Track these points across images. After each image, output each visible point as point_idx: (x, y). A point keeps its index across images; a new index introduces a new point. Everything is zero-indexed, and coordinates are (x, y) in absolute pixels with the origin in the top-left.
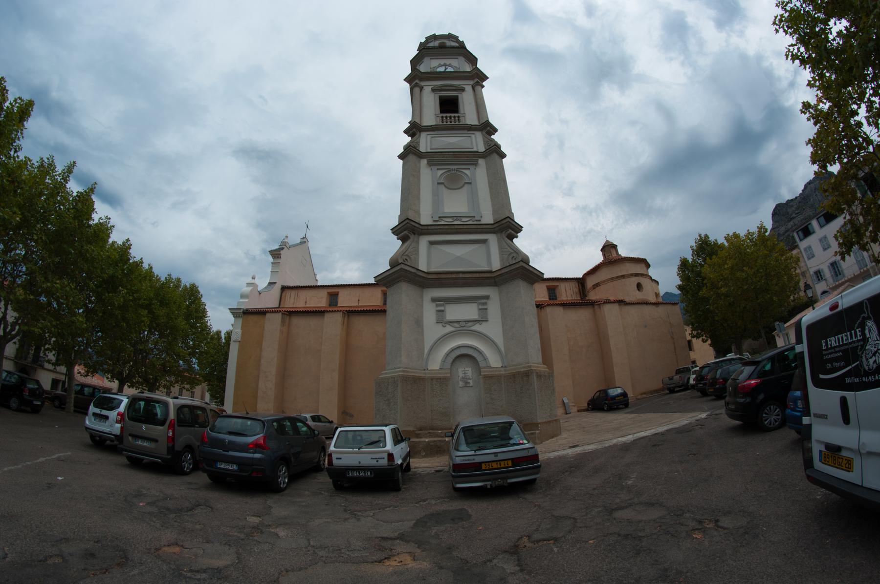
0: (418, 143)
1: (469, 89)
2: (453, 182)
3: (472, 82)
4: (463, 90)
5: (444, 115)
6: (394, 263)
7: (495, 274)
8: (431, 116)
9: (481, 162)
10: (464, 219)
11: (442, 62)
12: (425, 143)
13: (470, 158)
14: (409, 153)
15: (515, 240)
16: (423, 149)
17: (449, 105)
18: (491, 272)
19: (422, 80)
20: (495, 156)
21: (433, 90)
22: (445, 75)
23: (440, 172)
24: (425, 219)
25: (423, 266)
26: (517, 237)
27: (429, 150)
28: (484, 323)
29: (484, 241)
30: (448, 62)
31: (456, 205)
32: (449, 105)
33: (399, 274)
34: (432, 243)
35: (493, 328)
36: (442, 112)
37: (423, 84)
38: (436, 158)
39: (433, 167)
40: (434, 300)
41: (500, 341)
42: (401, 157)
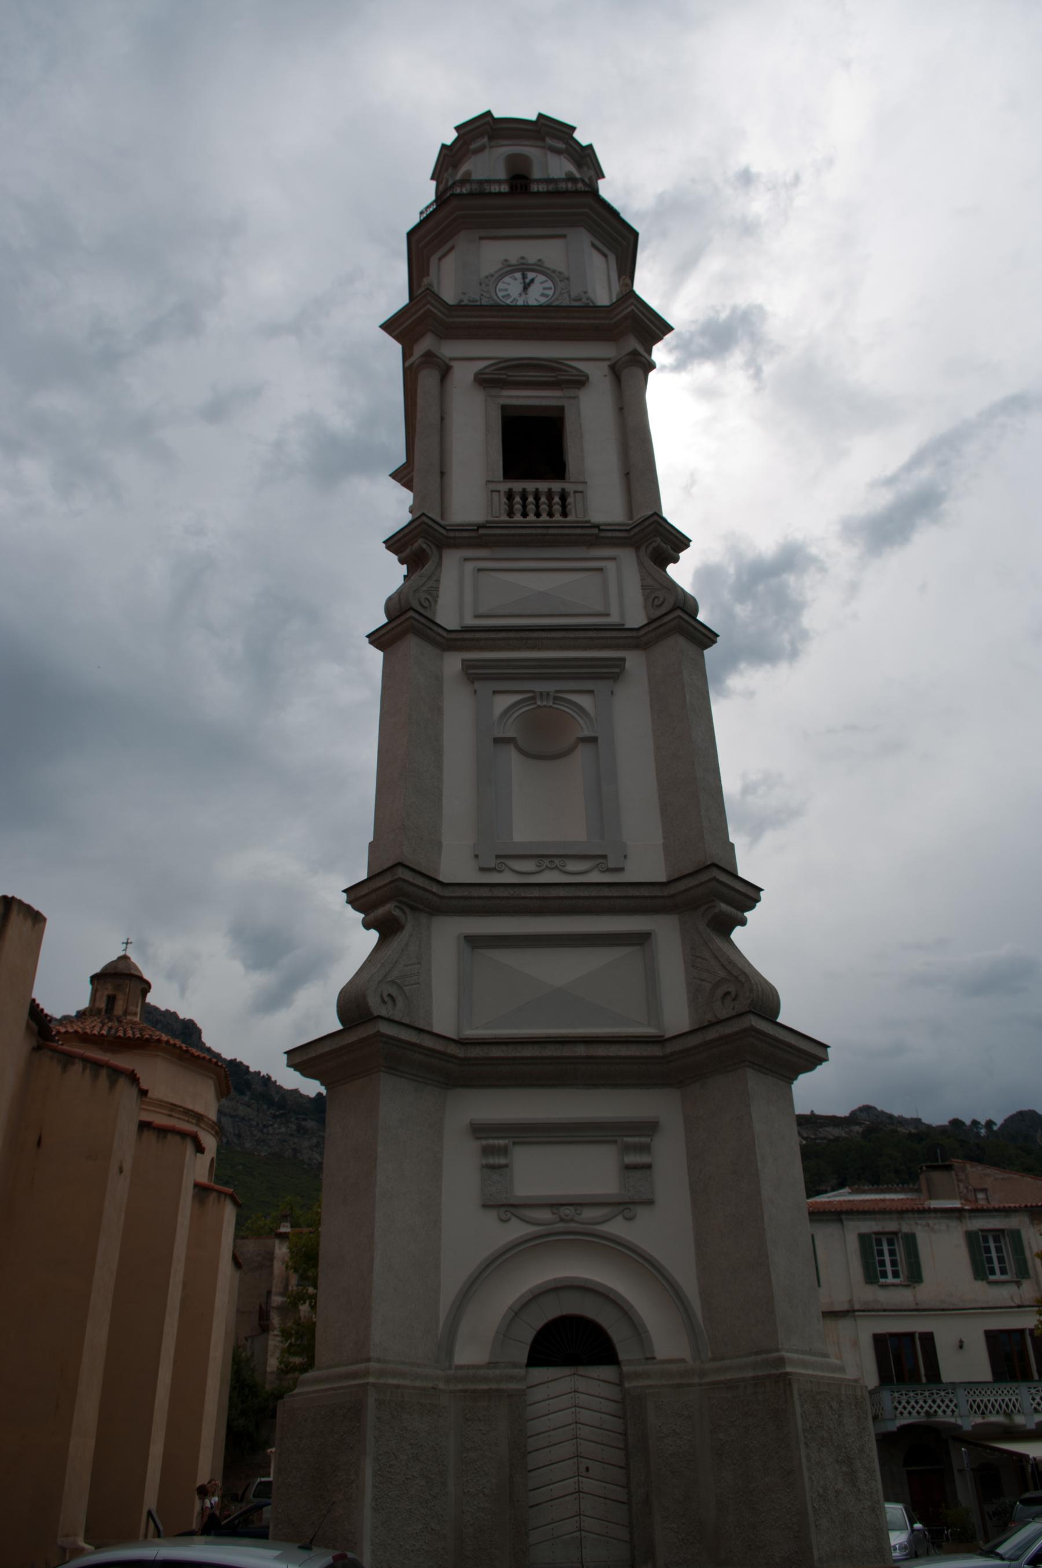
0: (433, 594)
1: (598, 374)
2: (544, 738)
3: (608, 351)
4: (580, 382)
5: (518, 486)
6: (352, 1006)
7: (670, 1048)
8: (473, 490)
9: (634, 661)
10: (572, 866)
11: (512, 250)
12: (463, 593)
13: (592, 653)
14: (403, 628)
15: (738, 935)
16: (448, 615)
17: (534, 446)
18: (658, 1041)
19: (450, 332)
20: (679, 642)
21: (485, 381)
22: (524, 283)
23: (503, 702)
24: (456, 865)
25: (443, 1018)
26: (743, 922)
27: (470, 621)
28: (642, 1212)
29: (641, 939)
30: (534, 250)
31: (544, 814)
32: (534, 446)
33: (368, 1041)
34: (475, 942)
35: (665, 1230)
36: (511, 471)
37: (449, 350)
38: (493, 651)
39: (478, 685)
40: (478, 1130)
41: (685, 1274)
42: (377, 639)
